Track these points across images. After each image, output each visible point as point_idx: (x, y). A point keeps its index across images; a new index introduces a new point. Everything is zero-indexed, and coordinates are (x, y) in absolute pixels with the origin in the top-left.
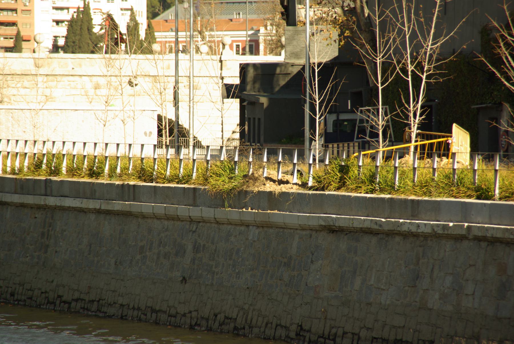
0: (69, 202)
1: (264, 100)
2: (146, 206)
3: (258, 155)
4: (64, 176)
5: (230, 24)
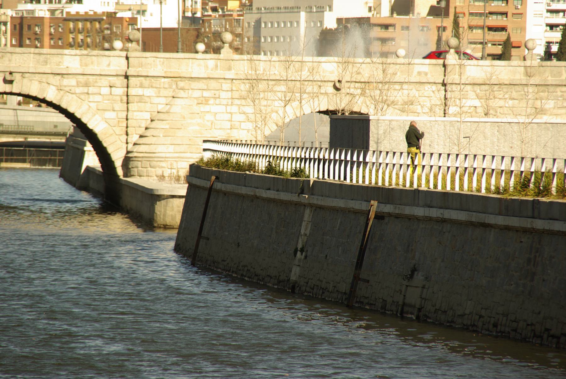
4: (553, 197)
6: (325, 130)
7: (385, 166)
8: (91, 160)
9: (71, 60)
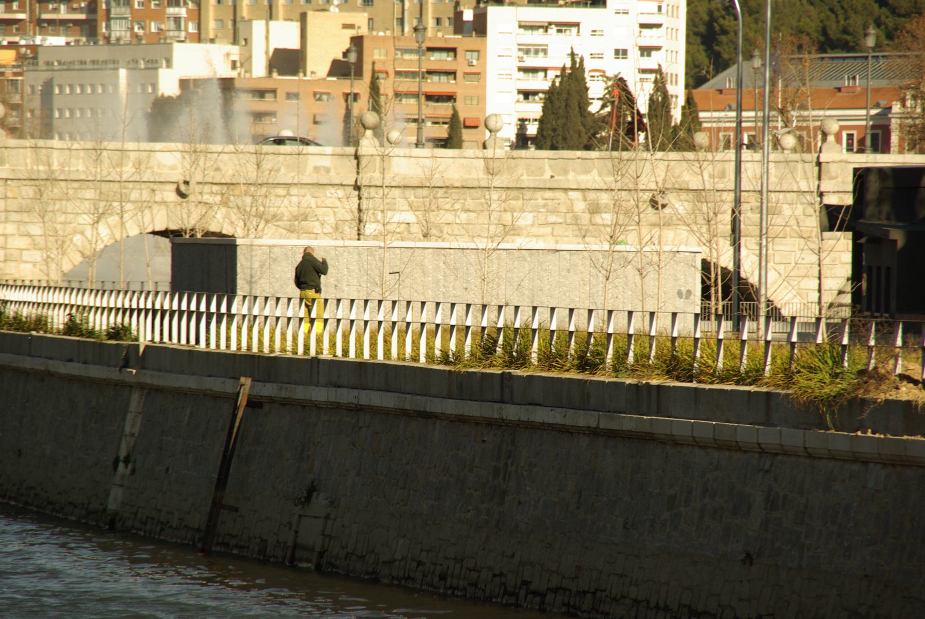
0: (541, 415)
1: (898, 236)
2: (681, 424)
3: (886, 337)
5: (839, 97)
6: (161, 263)
7: (263, 321)
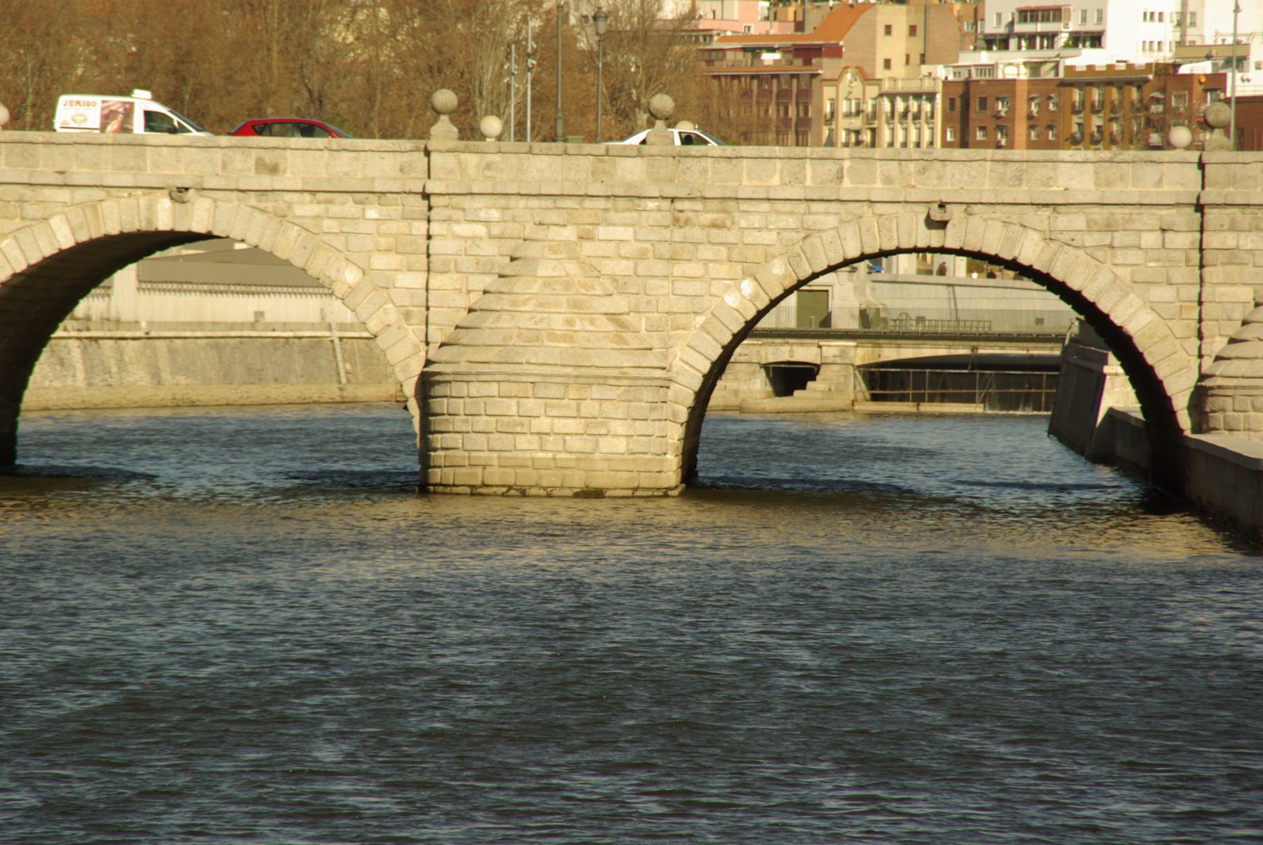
8: (1118, 394)
9: (1075, 173)
